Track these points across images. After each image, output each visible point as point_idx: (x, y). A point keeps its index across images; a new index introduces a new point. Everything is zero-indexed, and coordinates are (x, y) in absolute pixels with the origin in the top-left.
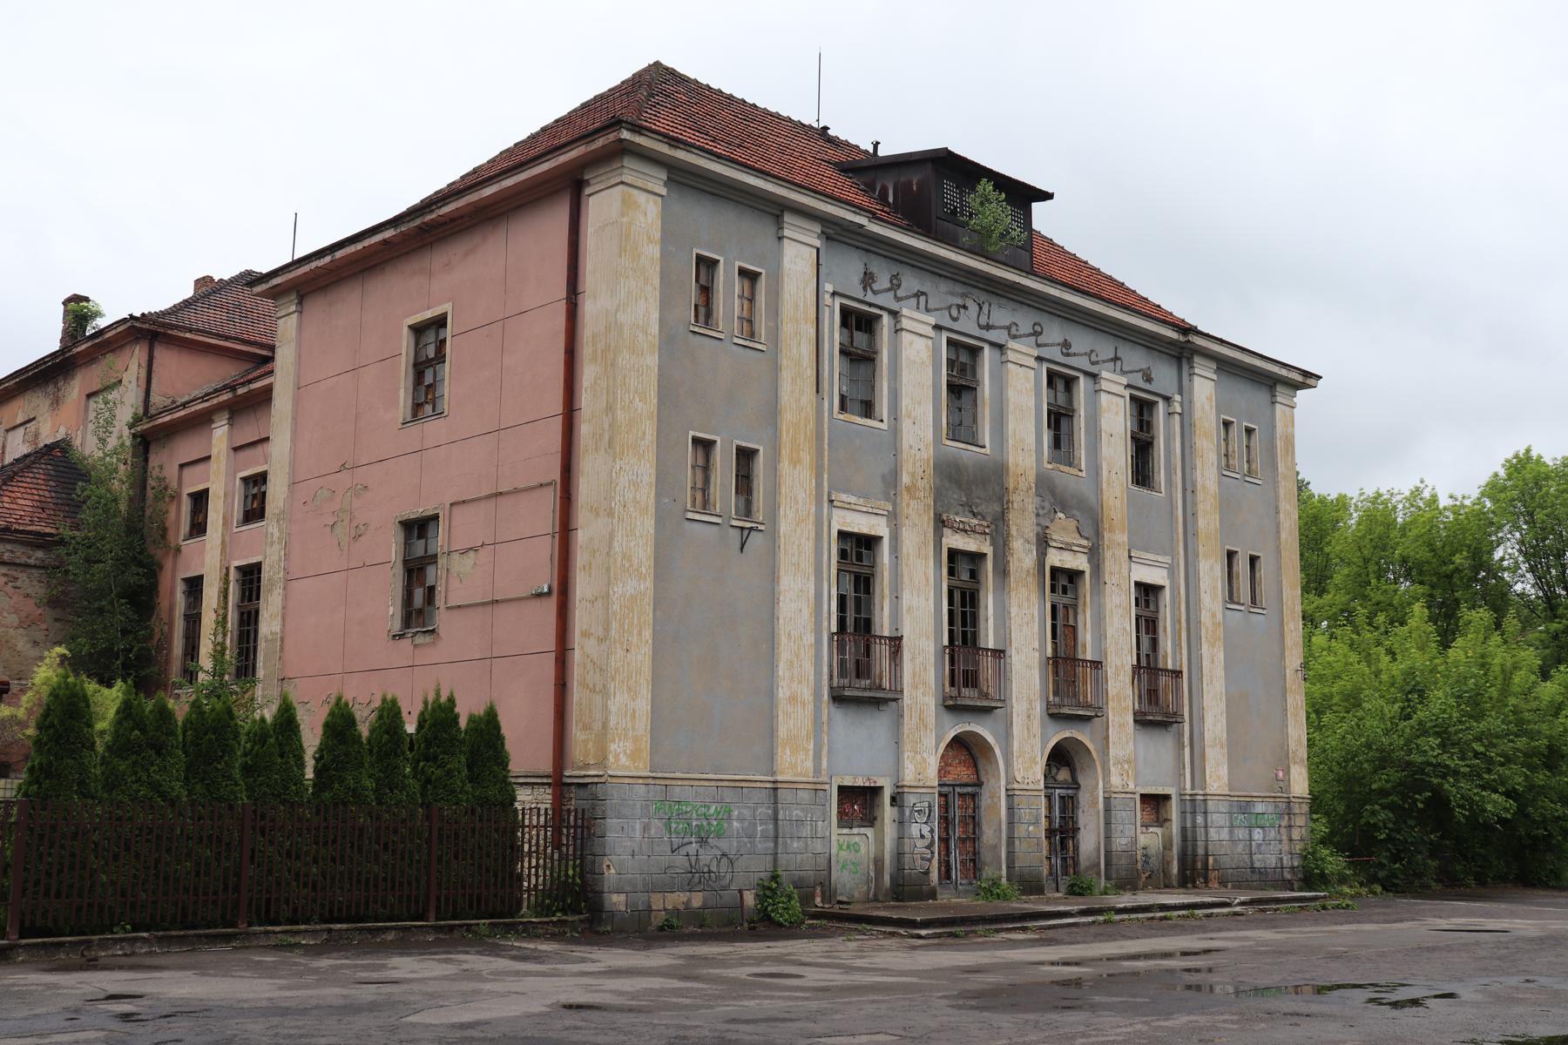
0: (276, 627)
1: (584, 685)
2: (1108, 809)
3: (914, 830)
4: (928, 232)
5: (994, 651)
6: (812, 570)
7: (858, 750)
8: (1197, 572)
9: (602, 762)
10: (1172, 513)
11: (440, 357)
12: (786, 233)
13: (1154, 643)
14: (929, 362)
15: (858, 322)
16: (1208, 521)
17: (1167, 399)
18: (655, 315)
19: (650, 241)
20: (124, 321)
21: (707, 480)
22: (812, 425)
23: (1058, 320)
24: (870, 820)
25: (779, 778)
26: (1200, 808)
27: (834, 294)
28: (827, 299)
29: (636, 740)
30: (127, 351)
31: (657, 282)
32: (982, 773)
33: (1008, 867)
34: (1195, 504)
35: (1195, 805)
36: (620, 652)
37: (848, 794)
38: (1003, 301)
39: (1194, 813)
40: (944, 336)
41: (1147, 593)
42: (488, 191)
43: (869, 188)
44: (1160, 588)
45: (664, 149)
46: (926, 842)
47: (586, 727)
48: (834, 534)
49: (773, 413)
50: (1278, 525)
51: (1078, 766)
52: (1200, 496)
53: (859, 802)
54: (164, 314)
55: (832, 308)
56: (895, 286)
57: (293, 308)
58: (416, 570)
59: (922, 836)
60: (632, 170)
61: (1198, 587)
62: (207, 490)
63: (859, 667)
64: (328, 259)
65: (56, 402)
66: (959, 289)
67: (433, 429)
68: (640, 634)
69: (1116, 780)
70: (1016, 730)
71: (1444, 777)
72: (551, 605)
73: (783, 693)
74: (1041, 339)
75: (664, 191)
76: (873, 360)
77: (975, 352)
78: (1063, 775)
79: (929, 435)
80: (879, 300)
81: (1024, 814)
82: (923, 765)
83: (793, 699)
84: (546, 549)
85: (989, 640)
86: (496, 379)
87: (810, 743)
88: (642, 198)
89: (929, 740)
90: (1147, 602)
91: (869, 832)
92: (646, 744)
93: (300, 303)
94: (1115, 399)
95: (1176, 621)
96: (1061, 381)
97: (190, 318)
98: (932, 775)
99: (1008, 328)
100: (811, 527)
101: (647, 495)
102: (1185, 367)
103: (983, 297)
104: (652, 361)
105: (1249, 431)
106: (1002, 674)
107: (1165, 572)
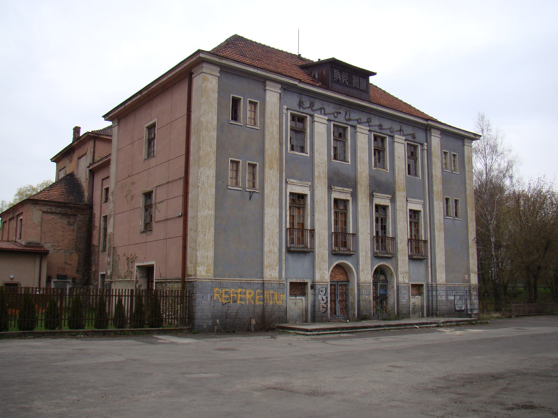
0: (111, 231)
1: (190, 247)
2: (398, 290)
3: (320, 297)
4: (327, 88)
5: (352, 234)
6: (278, 206)
7: (298, 270)
8: (433, 205)
9: (195, 275)
10: (424, 185)
11: (154, 138)
12: (267, 88)
13: (417, 231)
14: (326, 133)
15: (299, 119)
16: (437, 187)
17: (422, 145)
18: (215, 118)
19: (213, 92)
21: (237, 175)
22: (278, 155)
23: (377, 117)
24: (304, 294)
25: (265, 279)
26: (434, 288)
27: (287, 109)
28: (285, 111)
29: (208, 266)
31: (216, 106)
32: (349, 277)
33: (358, 310)
34: (432, 181)
35: (432, 288)
36: (202, 236)
37: (293, 285)
38: (355, 111)
39: (432, 291)
40: (332, 123)
41: (414, 214)
43: (309, 75)
44: (420, 211)
46: (325, 301)
47: (191, 262)
48: (288, 194)
49: (262, 151)
50: (465, 188)
51: (387, 275)
52: (434, 178)
53: (298, 288)
54: (101, 131)
56: (312, 105)
58: (148, 207)
59: (323, 300)
61: (433, 211)
63: (298, 242)
64: (123, 106)
65: (71, 161)
66: (338, 106)
67: (153, 161)
68: (209, 229)
69: (401, 279)
70: (361, 262)
71: (210, 270)
72: (182, 220)
73: (266, 249)
74: (370, 124)
75: (219, 75)
76: (304, 132)
77: (345, 129)
79: (326, 158)
80: (306, 111)
81: (364, 291)
82: (323, 273)
83: (270, 251)
84: (180, 200)
85: (390, 234)
86: (169, 142)
87: (274, 266)
88: (210, 77)
89: (326, 266)
90: (415, 216)
91: (303, 298)
92: (212, 268)
93: (118, 122)
94: (400, 145)
95: (425, 223)
96: (379, 139)
99: (357, 120)
100: (278, 191)
101: (213, 181)
103: (348, 109)
104: (214, 134)
105: (454, 156)
106: (356, 243)
107: (421, 206)
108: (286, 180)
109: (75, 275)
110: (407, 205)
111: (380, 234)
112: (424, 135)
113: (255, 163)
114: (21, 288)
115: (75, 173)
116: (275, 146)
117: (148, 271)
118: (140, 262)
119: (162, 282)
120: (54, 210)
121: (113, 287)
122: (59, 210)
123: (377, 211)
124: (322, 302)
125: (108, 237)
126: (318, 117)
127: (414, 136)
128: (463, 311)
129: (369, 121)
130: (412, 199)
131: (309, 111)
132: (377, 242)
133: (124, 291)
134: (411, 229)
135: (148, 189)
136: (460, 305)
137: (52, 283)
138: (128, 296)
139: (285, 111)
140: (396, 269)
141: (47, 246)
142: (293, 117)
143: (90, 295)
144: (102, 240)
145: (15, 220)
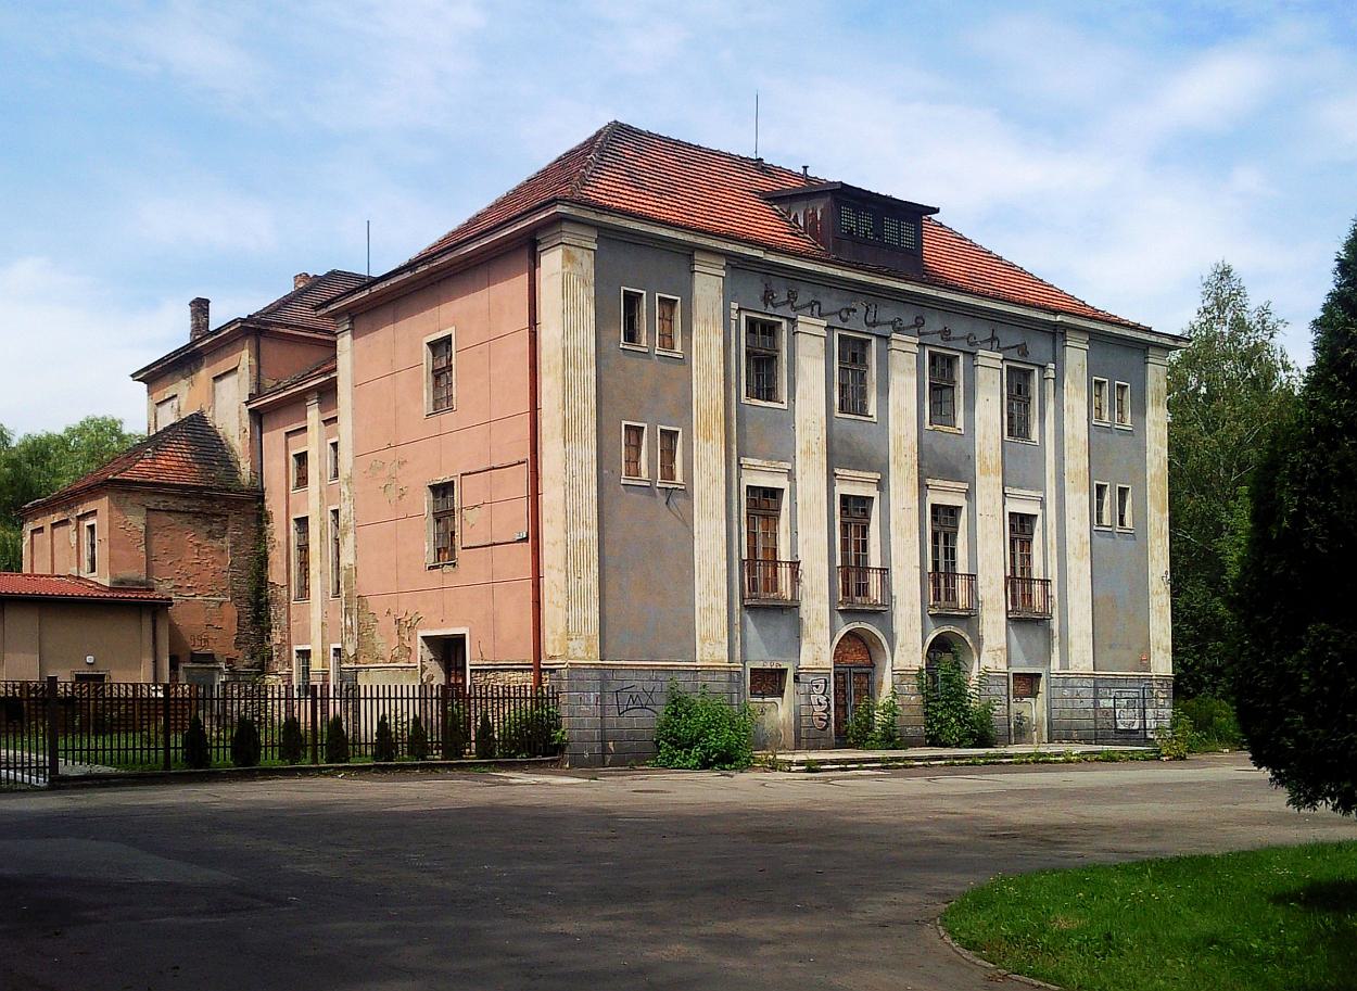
20: (234, 322)
22: (721, 410)
27: (740, 309)
28: (734, 315)
29: (588, 638)
30: (239, 344)
42: (472, 248)
45: (591, 216)
53: (769, 681)
55: (738, 322)
56: (792, 297)
57: (347, 326)
58: (443, 516)
59: (820, 704)
60: (569, 234)
62: (306, 452)
63: (763, 596)
64: (367, 292)
66: (847, 295)
77: (865, 343)
78: (947, 657)
82: (817, 649)
84: (523, 507)
86: (486, 380)
87: (712, 636)
90: (1023, 527)
93: (352, 323)
97: (288, 315)
98: (827, 660)
99: (893, 323)
102: (1059, 340)
108: (739, 460)
109: (234, 652)
110: (1004, 504)
111: (942, 568)
112: (1050, 346)
113: (676, 429)
114: (112, 685)
115: (208, 415)
116: (714, 392)
117: (449, 650)
118: (431, 629)
119: (486, 670)
120: (171, 504)
121: (361, 682)
122: (183, 504)
123: (934, 519)
124: (817, 709)
125: (343, 573)
126: (806, 323)
127: (1023, 350)
128: (1136, 732)
129: (919, 322)
130: (1016, 491)
131: (786, 311)
132: (936, 583)
133: (393, 689)
134: (1013, 556)
135: (441, 479)
136: (1127, 719)
137: (181, 672)
138: (366, 699)
139: (734, 315)
140: (979, 641)
141: (163, 589)
142: (752, 324)
143: (360, 698)
144: (294, 573)
145: (72, 527)
